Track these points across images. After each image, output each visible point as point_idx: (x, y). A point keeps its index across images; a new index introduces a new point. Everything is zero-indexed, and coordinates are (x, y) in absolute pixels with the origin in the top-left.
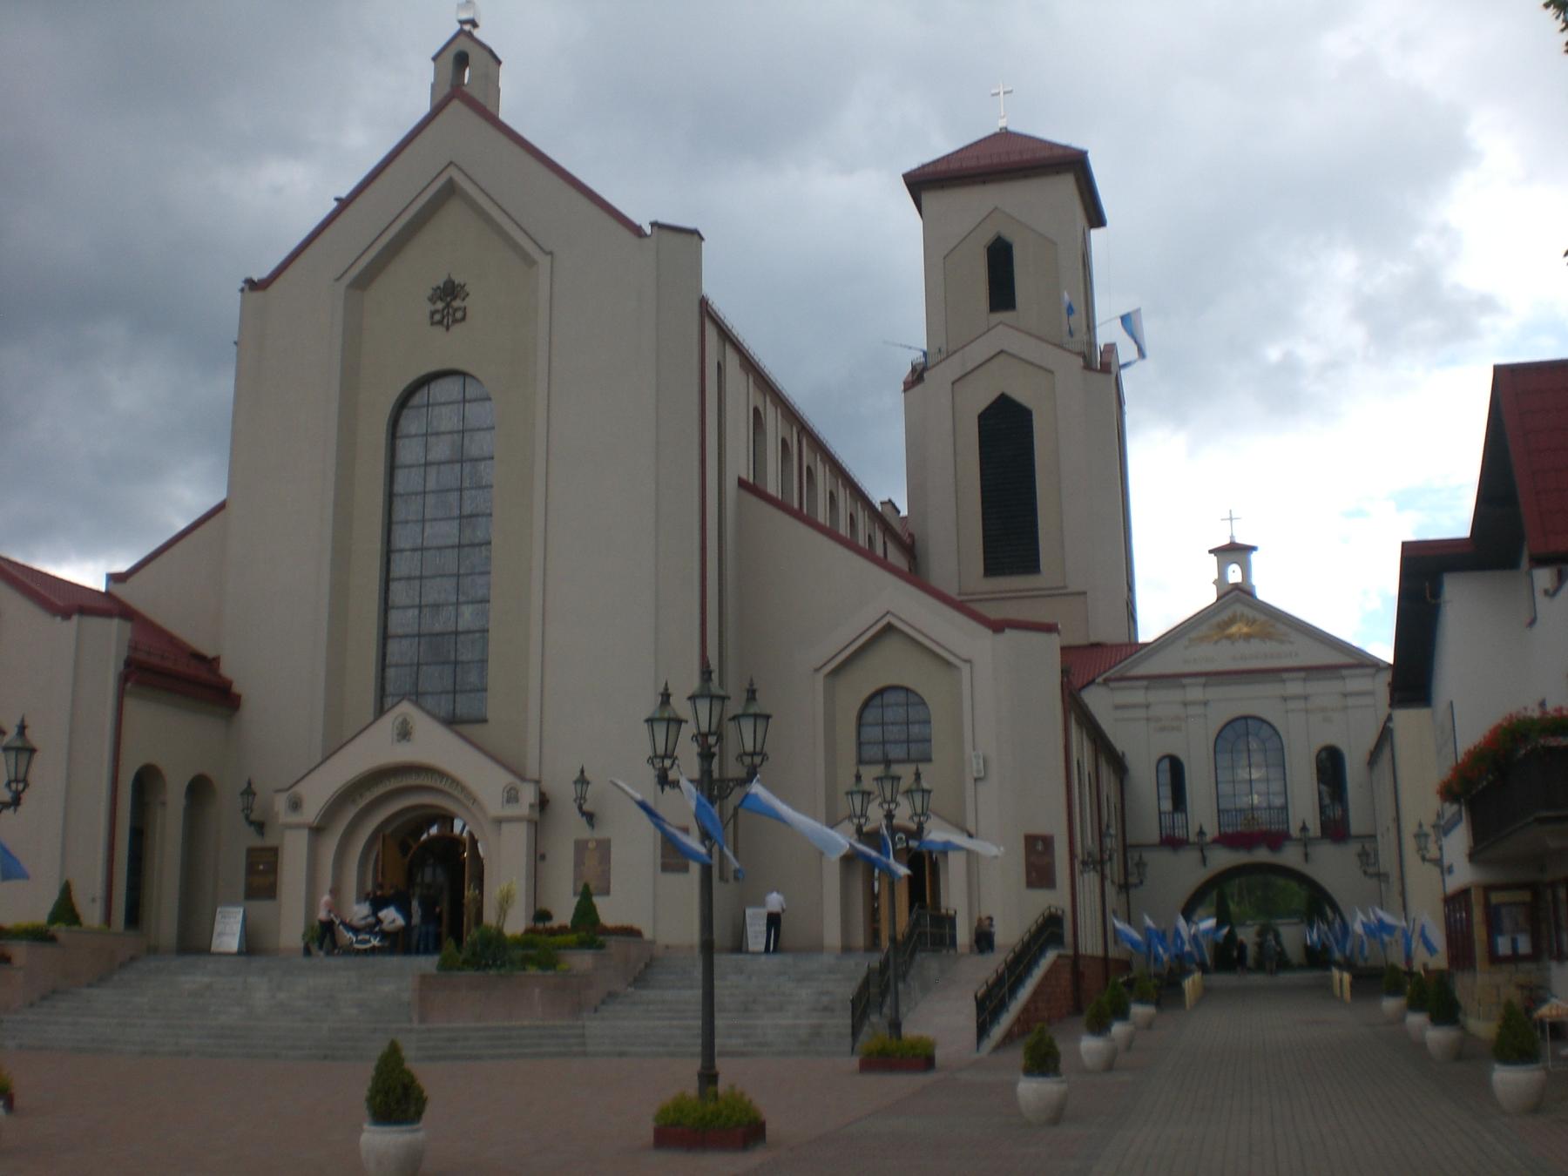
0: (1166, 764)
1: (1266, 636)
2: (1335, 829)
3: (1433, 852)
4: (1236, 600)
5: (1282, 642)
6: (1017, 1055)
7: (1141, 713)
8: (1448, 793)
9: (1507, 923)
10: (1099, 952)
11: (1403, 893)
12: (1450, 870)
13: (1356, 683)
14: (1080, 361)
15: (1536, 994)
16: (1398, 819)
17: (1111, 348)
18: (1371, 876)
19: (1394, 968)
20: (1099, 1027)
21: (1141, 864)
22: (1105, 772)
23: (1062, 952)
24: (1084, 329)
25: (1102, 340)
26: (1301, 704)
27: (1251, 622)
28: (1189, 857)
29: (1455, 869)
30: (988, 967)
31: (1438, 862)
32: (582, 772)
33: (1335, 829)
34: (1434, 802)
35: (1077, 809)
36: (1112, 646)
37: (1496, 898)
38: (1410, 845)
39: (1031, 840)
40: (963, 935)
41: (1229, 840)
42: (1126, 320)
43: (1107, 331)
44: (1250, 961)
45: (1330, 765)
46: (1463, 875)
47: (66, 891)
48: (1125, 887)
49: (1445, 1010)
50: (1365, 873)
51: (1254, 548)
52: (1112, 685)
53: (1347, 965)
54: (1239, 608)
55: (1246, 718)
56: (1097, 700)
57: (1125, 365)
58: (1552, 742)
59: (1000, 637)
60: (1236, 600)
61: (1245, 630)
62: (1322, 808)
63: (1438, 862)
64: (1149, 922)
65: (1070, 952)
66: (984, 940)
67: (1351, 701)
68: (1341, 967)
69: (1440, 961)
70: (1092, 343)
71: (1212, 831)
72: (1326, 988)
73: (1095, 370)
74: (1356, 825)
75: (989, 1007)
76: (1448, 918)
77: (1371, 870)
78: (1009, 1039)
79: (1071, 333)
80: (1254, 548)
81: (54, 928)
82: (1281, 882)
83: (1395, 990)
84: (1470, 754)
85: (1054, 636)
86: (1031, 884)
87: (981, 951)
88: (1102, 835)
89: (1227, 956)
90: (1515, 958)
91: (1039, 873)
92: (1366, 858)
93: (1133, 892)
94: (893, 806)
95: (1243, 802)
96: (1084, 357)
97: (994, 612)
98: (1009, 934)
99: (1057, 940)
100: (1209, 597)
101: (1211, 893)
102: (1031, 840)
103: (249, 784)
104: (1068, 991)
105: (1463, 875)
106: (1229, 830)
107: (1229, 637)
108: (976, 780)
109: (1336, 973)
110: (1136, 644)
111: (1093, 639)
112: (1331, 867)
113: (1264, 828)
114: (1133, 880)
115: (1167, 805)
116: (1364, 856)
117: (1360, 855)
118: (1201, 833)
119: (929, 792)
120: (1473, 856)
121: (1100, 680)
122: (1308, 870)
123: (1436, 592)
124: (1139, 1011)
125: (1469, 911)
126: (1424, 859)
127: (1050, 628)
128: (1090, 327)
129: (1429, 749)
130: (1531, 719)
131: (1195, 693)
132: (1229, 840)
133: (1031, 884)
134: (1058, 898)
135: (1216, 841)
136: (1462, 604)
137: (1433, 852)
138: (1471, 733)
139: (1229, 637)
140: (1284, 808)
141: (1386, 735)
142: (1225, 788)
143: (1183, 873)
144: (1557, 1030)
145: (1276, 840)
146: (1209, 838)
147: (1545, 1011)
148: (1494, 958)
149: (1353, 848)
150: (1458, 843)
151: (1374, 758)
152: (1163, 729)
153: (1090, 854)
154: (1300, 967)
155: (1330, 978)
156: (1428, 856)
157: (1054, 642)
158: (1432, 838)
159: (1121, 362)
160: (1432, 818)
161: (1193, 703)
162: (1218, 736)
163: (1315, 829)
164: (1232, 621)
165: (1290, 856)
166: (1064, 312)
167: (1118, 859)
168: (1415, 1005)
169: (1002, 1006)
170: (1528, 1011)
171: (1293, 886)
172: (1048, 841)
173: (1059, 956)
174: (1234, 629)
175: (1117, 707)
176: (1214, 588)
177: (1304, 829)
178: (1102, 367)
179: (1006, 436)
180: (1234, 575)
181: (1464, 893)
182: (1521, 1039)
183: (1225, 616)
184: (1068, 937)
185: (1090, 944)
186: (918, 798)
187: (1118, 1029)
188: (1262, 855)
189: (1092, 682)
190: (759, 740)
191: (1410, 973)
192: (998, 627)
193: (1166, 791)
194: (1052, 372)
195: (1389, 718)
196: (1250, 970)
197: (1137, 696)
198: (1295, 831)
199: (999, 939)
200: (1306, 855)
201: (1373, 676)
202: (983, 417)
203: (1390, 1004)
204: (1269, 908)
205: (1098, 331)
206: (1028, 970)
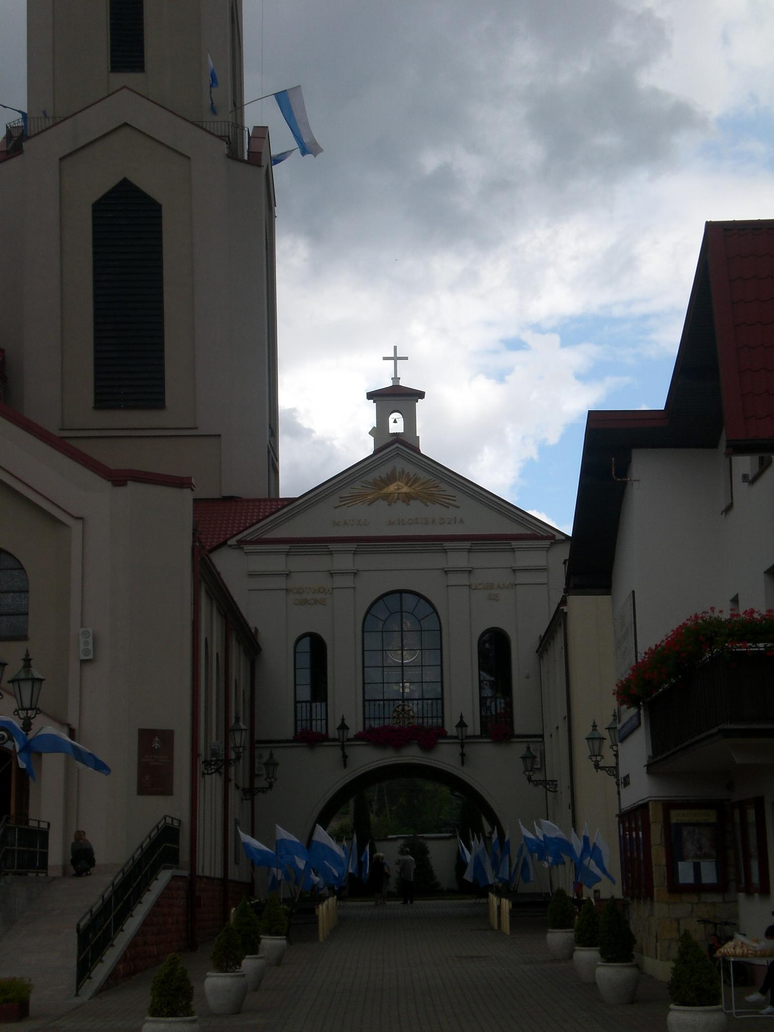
0: (306, 644)
1: (429, 498)
2: (498, 727)
3: (608, 760)
4: (397, 454)
5: (447, 506)
6: (142, 995)
7: (281, 583)
8: (627, 694)
9: (690, 848)
10: (219, 874)
11: (573, 806)
12: (626, 782)
13: (534, 558)
14: (224, 147)
15: (723, 930)
16: (569, 718)
17: (262, 133)
18: (537, 783)
19: (561, 893)
20: (227, 961)
21: (271, 764)
22: (236, 651)
23: (179, 873)
24: (230, 103)
25: (251, 120)
26: (463, 579)
27: (411, 481)
28: (328, 755)
29: (632, 780)
30: (96, 889)
31: (613, 771)
32: (461, 717)
33: (498, 727)
34: (612, 703)
35: (202, 698)
36: (248, 501)
37: (676, 816)
38: (582, 750)
39: (146, 736)
40: (57, 853)
41: (374, 737)
42: (283, 99)
43: (259, 112)
44: (392, 885)
45: (495, 649)
46: (641, 789)
48: (250, 793)
49: (619, 945)
50: (529, 779)
51: (421, 395)
52: (247, 548)
53: (505, 890)
54: (400, 464)
55: (401, 592)
56: (230, 565)
57: (277, 160)
58: (739, 647)
59: (120, 490)
60: (397, 454)
61: (405, 489)
62: (483, 700)
63: (613, 771)
64: (283, 834)
66: (82, 858)
67: (522, 578)
68: (500, 894)
69: (610, 887)
70: (238, 125)
71: (355, 726)
72: (482, 917)
73: (242, 161)
75: (92, 940)
76: (622, 839)
77: (536, 776)
78: (114, 980)
79: (214, 111)
80: (421, 395)
81: (326, 891)
82: (429, 786)
83: (561, 924)
84: (652, 653)
85: (187, 491)
86: (142, 790)
87: (80, 873)
88: (228, 731)
89: (365, 884)
90: (698, 888)
91: (153, 778)
92: (533, 763)
94: (599, 758)
95: (393, 690)
96: (229, 143)
97: (114, 463)
98: (113, 850)
99: (171, 858)
100: (365, 448)
101: (352, 804)
102: (146, 736)
103: (343, 720)
104: (186, 918)
105: (641, 789)
106: (376, 724)
107: (386, 497)
108: (83, 662)
109: (493, 899)
110: (278, 500)
111: (226, 493)
112: (492, 772)
113: (416, 722)
115: (305, 693)
116: (528, 758)
117: (524, 758)
118: (343, 727)
119: (41, 680)
120: (652, 768)
121: (233, 542)
122: (465, 774)
123: (624, 470)
124: (270, 943)
125: (646, 829)
126: (597, 766)
127: (183, 483)
128: (238, 105)
129: (605, 645)
130: (718, 620)
131: (344, 561)
132: (374, 737)
133: (142, 790)
134: (173, 807)
135: (359, 737)
136: (652, 486)
137: (608, 760)
138: (654, 632)
139: (386, 497)
140: (440, 699)
141: (559, 619)
142: (374, 675)
143: (321, 775)
144: (743, 973)
145: (430, 737)
146: (351, 734)
147: (728, 948)
148: (675, 888)
149: (519, 749)
150: (636, 751)
151: (545, 644)
152: (304, 602)
153: (214, 753)
154: (449, 893)
155: (487, 904)
156: (601, 764)
157: (187, 496)
158: (607, 743)
159: (275, 152)
160: (609, 720)
161: (342, 573)
162: (368, 612)
163: (474, 727)
164: (391, 478)
165: (445, 757)
166: (207, 80)
167: (243, 759)
168: (585, 940)
169: (106, 941)
170: (712, 949)
171: (445, 791)
172: (167, 737)
173: (174, 878)
174: (392, 488)
175: (252, 575)
176: (371, 440)
177: (462, 725)
178: (251, 159)
179: (127, 231)
180: (396, 424)
181: (643, 807)
182: (698, 981)
183: (383, 472)
185: (209, 864)
186: (26, 688)
187: (249, 964)
188: (412, 755)
189: (224, 543)
190: (34, 699)
191: (579, 902)
192: (119, 478)
193: (305, 676)
194: (189, 158)
195: (563, 602)
196: (391, 896)
197: (276, 562)
198: (451, 728)
199: (100, 857)
200: (463, 755)
201: (548, 549)
202: (98, 207)
203: (557, 938)
204: (413, 817)
205: (246, 109)
206: (137, 897)
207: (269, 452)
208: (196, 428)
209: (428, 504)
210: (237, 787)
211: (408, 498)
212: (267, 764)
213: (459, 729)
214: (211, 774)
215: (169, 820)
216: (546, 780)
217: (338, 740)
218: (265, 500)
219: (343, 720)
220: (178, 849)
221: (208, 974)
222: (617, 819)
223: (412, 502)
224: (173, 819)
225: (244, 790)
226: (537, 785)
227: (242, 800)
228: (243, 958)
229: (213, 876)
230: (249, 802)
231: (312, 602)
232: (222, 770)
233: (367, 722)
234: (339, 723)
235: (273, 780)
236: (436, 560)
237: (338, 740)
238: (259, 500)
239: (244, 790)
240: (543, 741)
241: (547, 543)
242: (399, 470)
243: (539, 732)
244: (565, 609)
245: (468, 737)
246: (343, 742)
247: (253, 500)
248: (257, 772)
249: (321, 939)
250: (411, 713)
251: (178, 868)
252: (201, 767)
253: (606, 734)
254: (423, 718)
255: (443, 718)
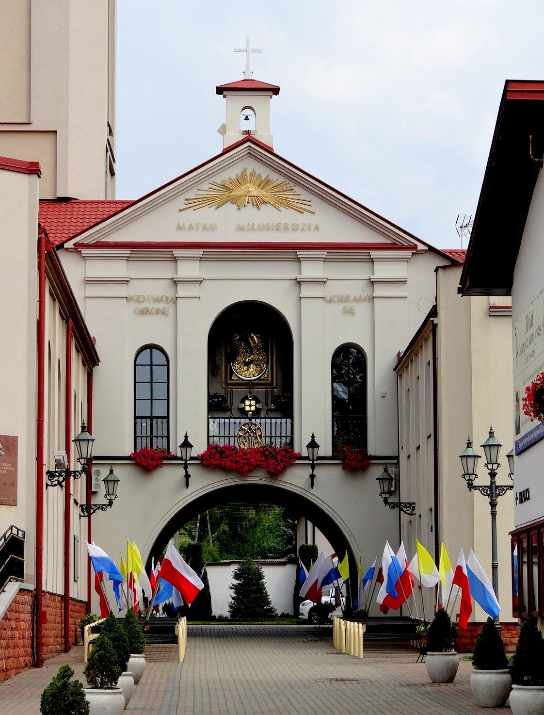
10: (60, 591)
18: (393, 506)
32: (313, 437)
36: (84, 203)
45: (349, 362)
47: (317, 580)
48: (88, 509)
50: (386, 501)
52: (85, 252)
56: (73, 269)
65: (32, 587)
67: (379, 291)
71: (199, 448)
74: (377, 442)
92: (391, 486)
93: (98, 517)
94: (495, 466)
99: (17, 570)
103: (186, 437)
111: (60, 194)
114: (100, 499)
121: (69, 245)
126: (471, 486)
131: (188, 269)
151: (403, 362)
152: (144, 312)
163: (325, 448)
165: (294, 480)
173: (21, 590)
177: (313, 445)
184: (29, 568)
187: (125, 680)
188: (258, 478)
197: (117, 268)
198: (301, 447)
200: (312, 477)
207: (107, 151)
208: (29, 124)
209: (281, 208)
210: (76, 503)
211: (258, 203)
212: (106, 481)
213: (310, 449)
214: (55, 485)
215: (15, 531)
216: (400, 503)
217: (181, 459)
218: (103, 203)
219: (186, 437)
220: (22, 563)
221: (543, 518)
222: (510, 537)
223: (263, 207)
224: (18, 530)
225: (81, 506)
226: (394, 507)
227: (80, 516)
228: (120, 675)
229: (55, 592)
230: (87, 518)
231: (154, 311)
232: (64, 484)
233: (211, 440)
234: (181, 440)
235: (113, 497)
236: (286, 270)
237: (181, 459)
238: (97, 203)
239: (81, 506)
240: (398, 464)
241: (408, 253)
242: (249, 171)
243: (395, 454)
244: (435, 320)
245: (319, 458)
246: (186, 461)
247: (91, 203)
248: (93, 490)
249: (181, 660)
250: (258, 433)
251: (23, 581)
252: (45, 478)
253: (480, 451)
254: (271, 437)
255: (292, 437)
